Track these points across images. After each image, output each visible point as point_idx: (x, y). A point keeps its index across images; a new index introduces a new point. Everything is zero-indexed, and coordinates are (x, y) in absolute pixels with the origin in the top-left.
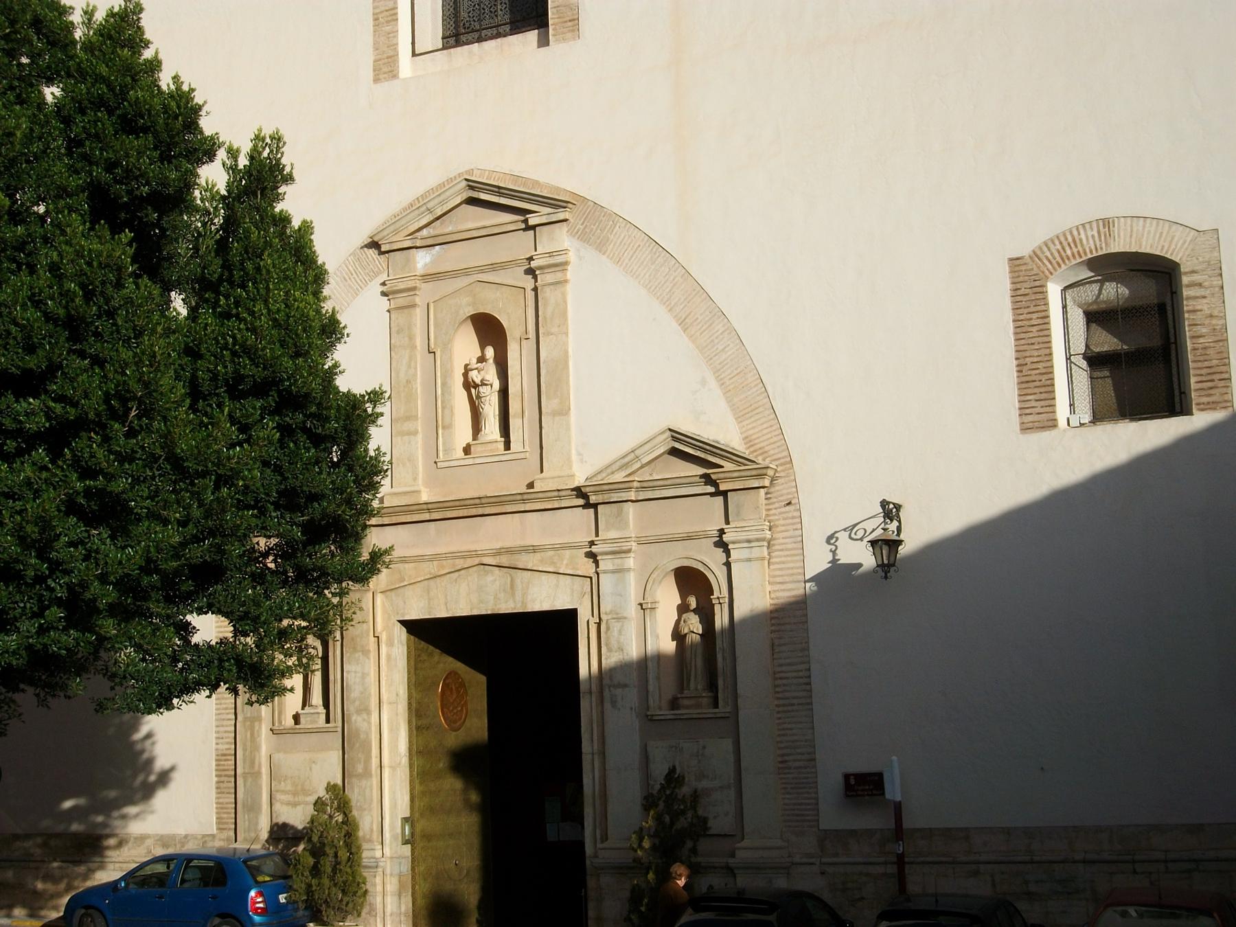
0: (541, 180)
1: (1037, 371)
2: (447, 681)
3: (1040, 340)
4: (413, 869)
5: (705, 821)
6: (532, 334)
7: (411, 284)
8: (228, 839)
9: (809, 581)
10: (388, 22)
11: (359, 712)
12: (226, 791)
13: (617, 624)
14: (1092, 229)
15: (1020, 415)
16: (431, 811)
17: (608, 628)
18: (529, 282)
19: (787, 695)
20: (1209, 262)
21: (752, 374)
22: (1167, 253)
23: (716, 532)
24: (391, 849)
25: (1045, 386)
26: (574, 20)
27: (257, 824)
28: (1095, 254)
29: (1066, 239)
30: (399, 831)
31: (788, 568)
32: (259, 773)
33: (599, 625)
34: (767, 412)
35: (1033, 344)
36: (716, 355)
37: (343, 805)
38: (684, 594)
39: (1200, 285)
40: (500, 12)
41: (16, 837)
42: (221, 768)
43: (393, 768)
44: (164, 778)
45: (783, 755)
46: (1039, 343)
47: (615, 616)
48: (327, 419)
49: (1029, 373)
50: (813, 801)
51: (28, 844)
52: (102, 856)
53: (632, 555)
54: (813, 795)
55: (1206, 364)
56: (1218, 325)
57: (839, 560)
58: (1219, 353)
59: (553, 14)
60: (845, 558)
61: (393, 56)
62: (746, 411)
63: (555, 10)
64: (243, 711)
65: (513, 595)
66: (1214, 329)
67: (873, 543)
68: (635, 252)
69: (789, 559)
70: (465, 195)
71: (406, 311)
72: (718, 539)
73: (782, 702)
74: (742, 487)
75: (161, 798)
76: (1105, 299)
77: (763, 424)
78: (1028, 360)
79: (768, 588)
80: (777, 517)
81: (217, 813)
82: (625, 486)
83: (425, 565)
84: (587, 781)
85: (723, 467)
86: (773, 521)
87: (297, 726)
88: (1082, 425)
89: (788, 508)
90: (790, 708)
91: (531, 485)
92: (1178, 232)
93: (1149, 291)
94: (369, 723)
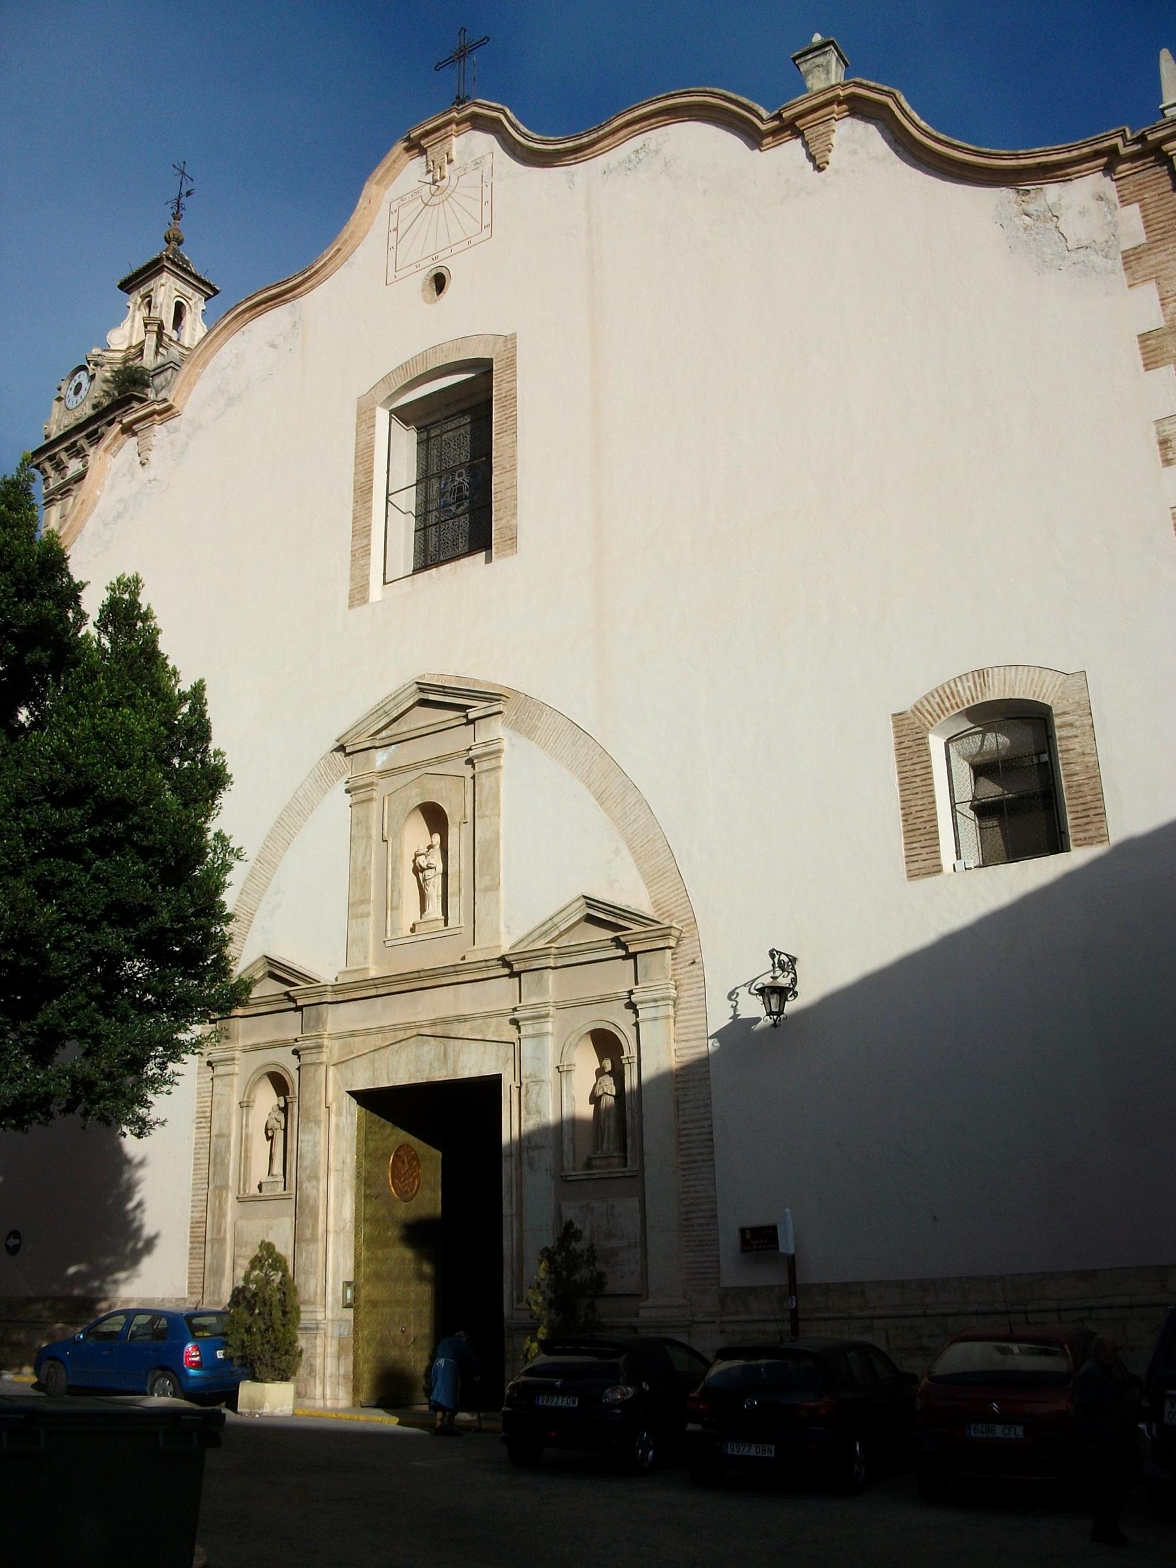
0: (481, 678)
1: (922, 820)
2: (399, 1153)
3: (924, 789)
4: (356, 1332)
6: (470, 819)
9: (711, 1037)
10: (363, 556)
11: (309, 1179)
12: (198, 1256)
13: (535, 1087)
14: (968, 680)
15: (906, 863)
16: (378, 1277)
17: (527, 1091)
18: (468, 771)
19: (692, 1151)
20: (1078, 703)
21: (661, 841)
22: (1038, 697)
23: (626, 994)
24: (333, 1312)
25: (929, 833)
26: (513, 538)
27: (220, 1287)
28: (972, 704)
29: (945, 692)
30: (340, 1294)
31: (693, 1026)
32: (224, 1240)
34: (674, 876)
35: (917, 793)
36: (628, 825)
38: (601, 1059)
40: (461, 544)
41: (30, 1301)
42: (195, 1234)
43: (337, 1233)
44: (150, 1244)
45: (687, 1213)
46: (923, 792)
47: (534, 1080)
49: (914, 821)
50: (715, 1259)
51: (40, 1306)
53: (551, 1019)
54: (715, 1252)
55: (1081, 800)
56: (1090, 762)
57: (739, 1015)
58: (1093, 789)
59: (496, 535)
60: (744, 1014)
61: (366, 584)
62: (655, 876)
63: (497, 532)
64: (214, 1180)
65: (446, 1063)
66: (1087, 766)
67: (761, 991)
68: (558, 737)
69: (693, 1016)
71: (365, 805)
72: (628, 1000)
73: (685, 1159)
74: (649, 948)
75: (147, 1264)
76: (988, 750)
77: (670, 888)
78: (913, 809)
79: (674, 1046)
80: (682, 977)
81: (189, 1278)
82: (543, 953)
83: (370, 1038)
84: (506, 1243)
85: (631, 929)
86: (678, 980)
87: (261, 1194)
89: (692, 967)
90: (693, 1165)
91: (463, 958)
92: (1048, 676)
94: (318, 1190)
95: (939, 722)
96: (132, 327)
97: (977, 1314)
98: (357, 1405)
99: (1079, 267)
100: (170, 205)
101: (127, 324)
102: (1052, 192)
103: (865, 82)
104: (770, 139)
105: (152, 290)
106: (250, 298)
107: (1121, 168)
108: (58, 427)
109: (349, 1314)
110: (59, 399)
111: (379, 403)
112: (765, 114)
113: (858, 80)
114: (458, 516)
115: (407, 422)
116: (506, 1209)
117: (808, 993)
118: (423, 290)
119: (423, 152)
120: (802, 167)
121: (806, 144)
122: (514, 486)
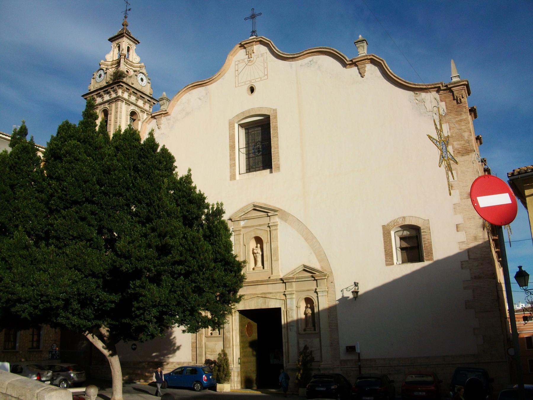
5: (314, 358)
7: (240, 229)
8: (194, 363)
11: (227, 332)
17: (289, 312)
28: (402, 225)
30: (238, 361)
33: (287, 311)
37: (225, 354)
39: (425, 232)
41: (141, 362)
43: (236, 346)
44: (178, 348)
48: (234, 267)
51: (144, 364)
52: (163, 367)
53: (294, 294)
55: (428, 250)
60: (345, 295)
67: (353, 292)
70: (253, 208)
75: (178, 353)
78: (387, 249)
79: (327, 302)
82: (293, 278)
88: (400, 264)
91: (269, 278)
93: (414, 233)
94: (230, 335)
95: (394, 228)
96: (113, 54)
97: (402, 366)
98: (242, 388)
99: (430, 116)
100: (123, 13)
101: (112, 53)
102: (423, 95)
103: (375, 56)
104: (348, 66)
105: (120, 42)
106: (192, 84)
107: (441, 92)
108: (94, 87)
109: (239, 366)
110: (93, 78)
111: (236, 122)
112: (348, 59)
113: (373, 55)
114: (259, 156)
115: (242, 127)
116: (284, 341)
117: (361, 291)
118: (247, 91)
119: (245, 48)
120: (358, 75)
121: (359, 69)
122: (278, 153)
